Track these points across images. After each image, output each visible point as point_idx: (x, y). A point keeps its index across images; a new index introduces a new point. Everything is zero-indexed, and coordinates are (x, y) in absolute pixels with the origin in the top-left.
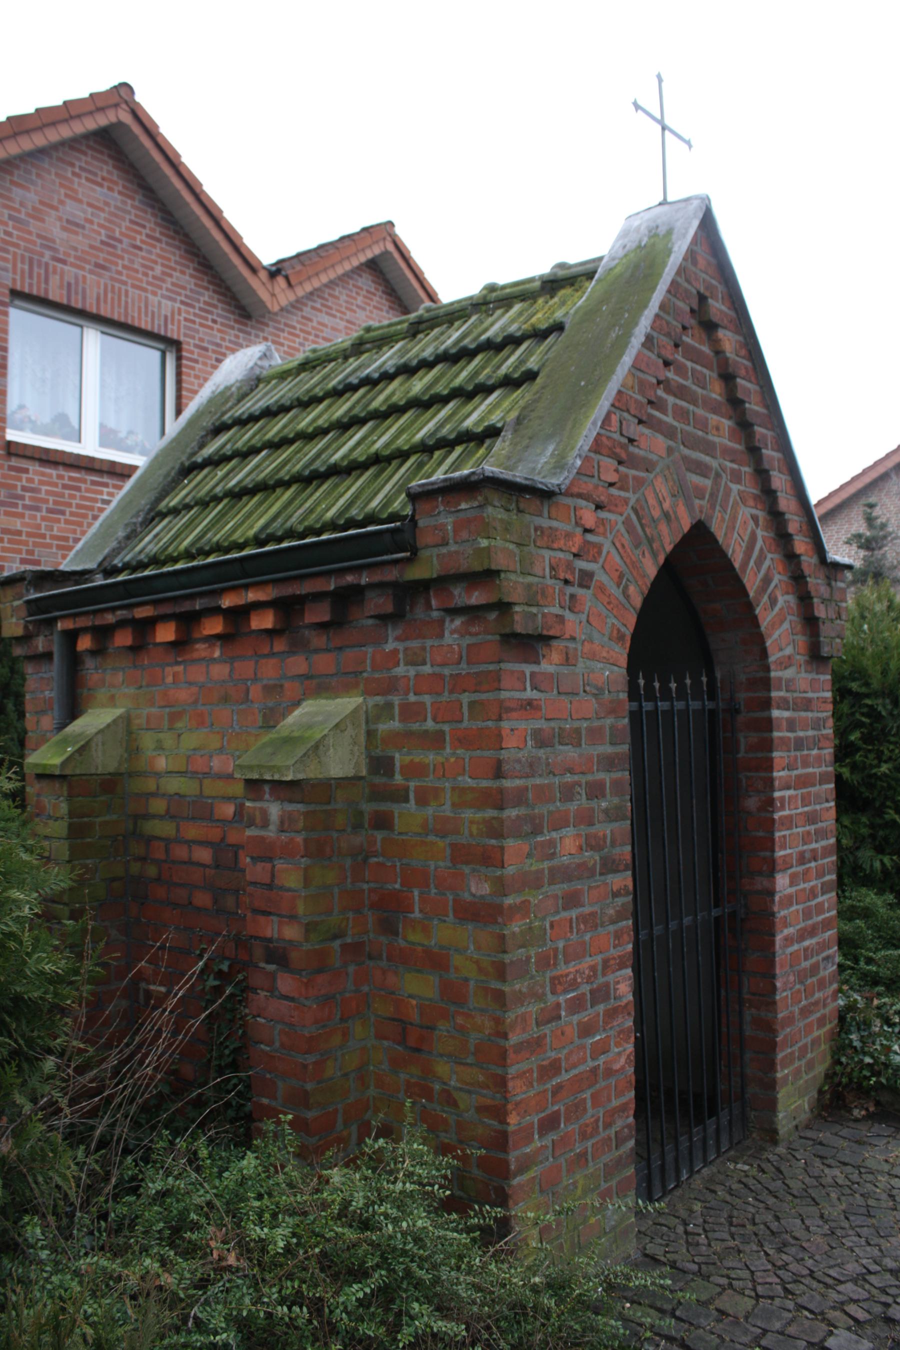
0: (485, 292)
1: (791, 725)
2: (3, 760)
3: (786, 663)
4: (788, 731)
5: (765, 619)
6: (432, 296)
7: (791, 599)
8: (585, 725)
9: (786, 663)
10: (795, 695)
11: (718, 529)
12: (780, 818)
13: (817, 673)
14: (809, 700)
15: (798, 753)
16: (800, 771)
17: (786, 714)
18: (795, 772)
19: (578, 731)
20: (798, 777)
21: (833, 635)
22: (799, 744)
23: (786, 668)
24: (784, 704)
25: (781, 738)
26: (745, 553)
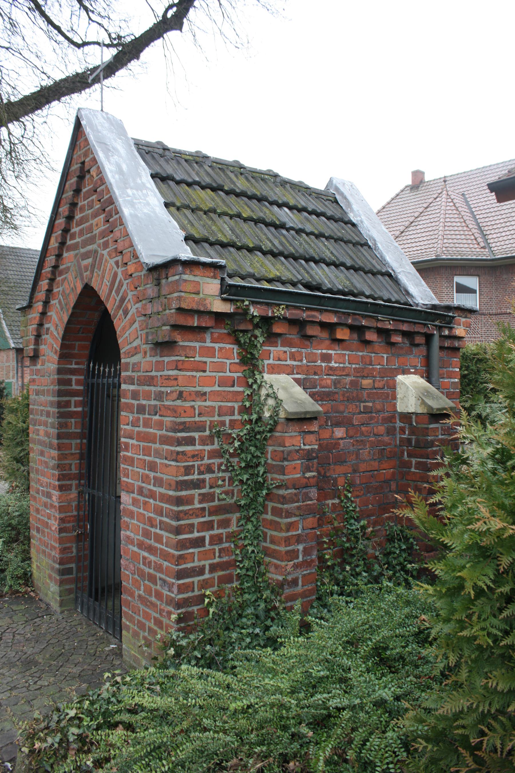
0: (108, 184)
1: (135, 395)
2: (371, 772)
3: (136, 351)
4: (132, 399)
5: (119, 326)
6: (36, 251)
7: (384, 271)
8: (46, 388)
9: (136, 351)
10: (139, 374)
11: (95, 285)
12: (124, 456)
13: (161, 357)
14: (152, 378)
15: (141, 416)
16: (141, 429)
17: (132, 387)
18: (137, 429)
19: (44, 390)
20: (139, 433)
21: (160, 324)
22: (141, 409)
23: (132, 356)
24: (131, 381)
25: (126, 403)
26: (109, 289)
